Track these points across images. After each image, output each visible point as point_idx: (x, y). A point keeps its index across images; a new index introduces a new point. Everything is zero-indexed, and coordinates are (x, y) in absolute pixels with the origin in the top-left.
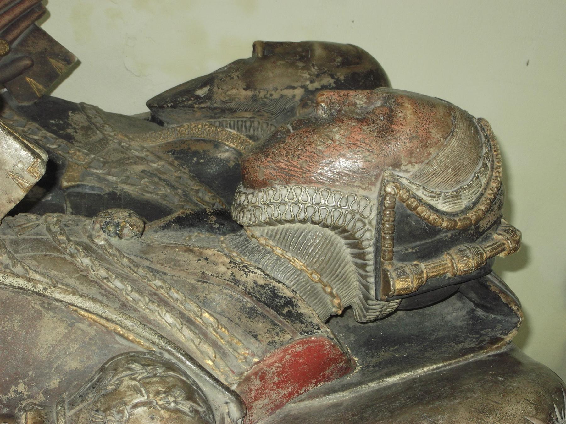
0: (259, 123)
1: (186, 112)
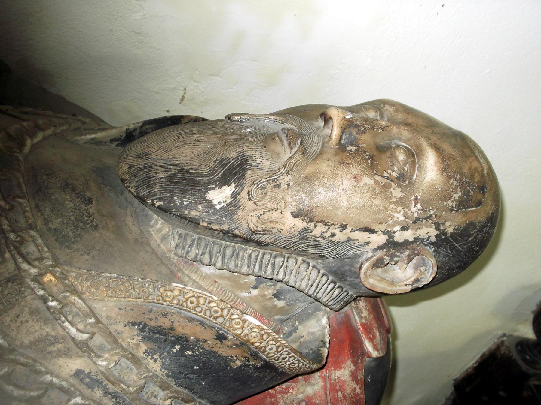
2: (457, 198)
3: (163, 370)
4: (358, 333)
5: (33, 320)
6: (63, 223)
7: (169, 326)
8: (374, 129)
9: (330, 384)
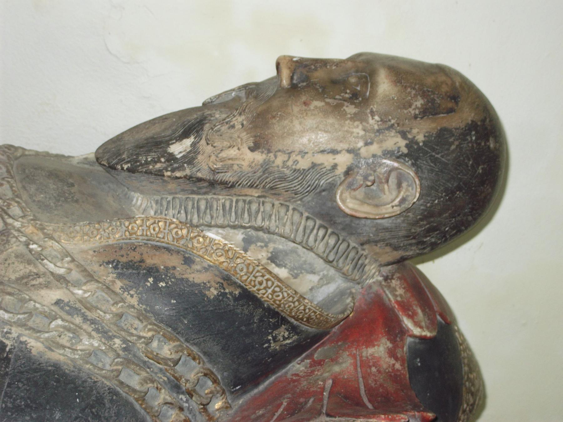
0: (273, 205)
1: (151, 180)
2: (419, 105)
3: (141, 305)
4: (394, 311)
5: (18, 261)
6: (46, 198)
7: (139, 259)
8: (326, 67)
9: (361, 361)
